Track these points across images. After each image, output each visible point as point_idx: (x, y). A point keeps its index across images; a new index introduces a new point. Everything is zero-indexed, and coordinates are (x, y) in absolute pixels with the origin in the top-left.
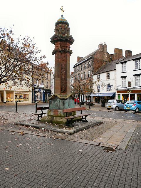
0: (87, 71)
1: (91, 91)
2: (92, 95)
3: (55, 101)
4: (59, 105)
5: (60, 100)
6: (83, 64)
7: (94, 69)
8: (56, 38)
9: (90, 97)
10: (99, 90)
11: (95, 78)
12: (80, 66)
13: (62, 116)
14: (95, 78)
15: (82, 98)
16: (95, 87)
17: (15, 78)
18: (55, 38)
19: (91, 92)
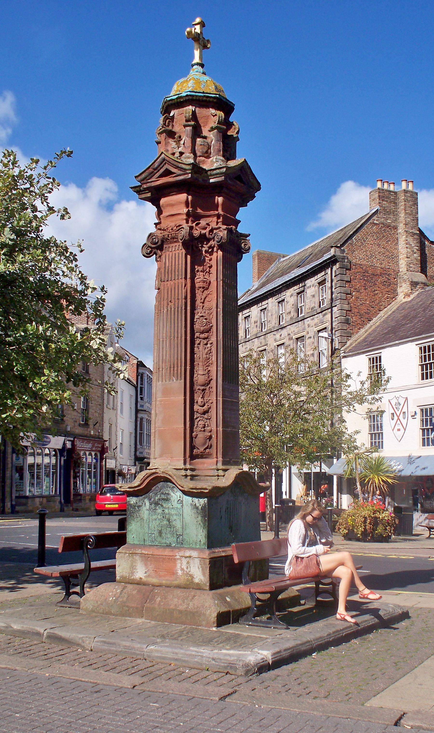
0: (313, 330)
1: (332, 445)
2: (337, 468)
3: (157, 504)
4: (178, 524)
5: (188, 499)
6: (289, 295)
7: (347, 322)
8: (167, 173)
9: (329, 478)
10: (376, 435)
11: (356, 367)
12: (271, 302)
13: (196, 581)
14: (356, 367)
15: (285, 487)
16: (355, 423)
17: (342, 443)
18: (161, 176)
19: (335, 453)
